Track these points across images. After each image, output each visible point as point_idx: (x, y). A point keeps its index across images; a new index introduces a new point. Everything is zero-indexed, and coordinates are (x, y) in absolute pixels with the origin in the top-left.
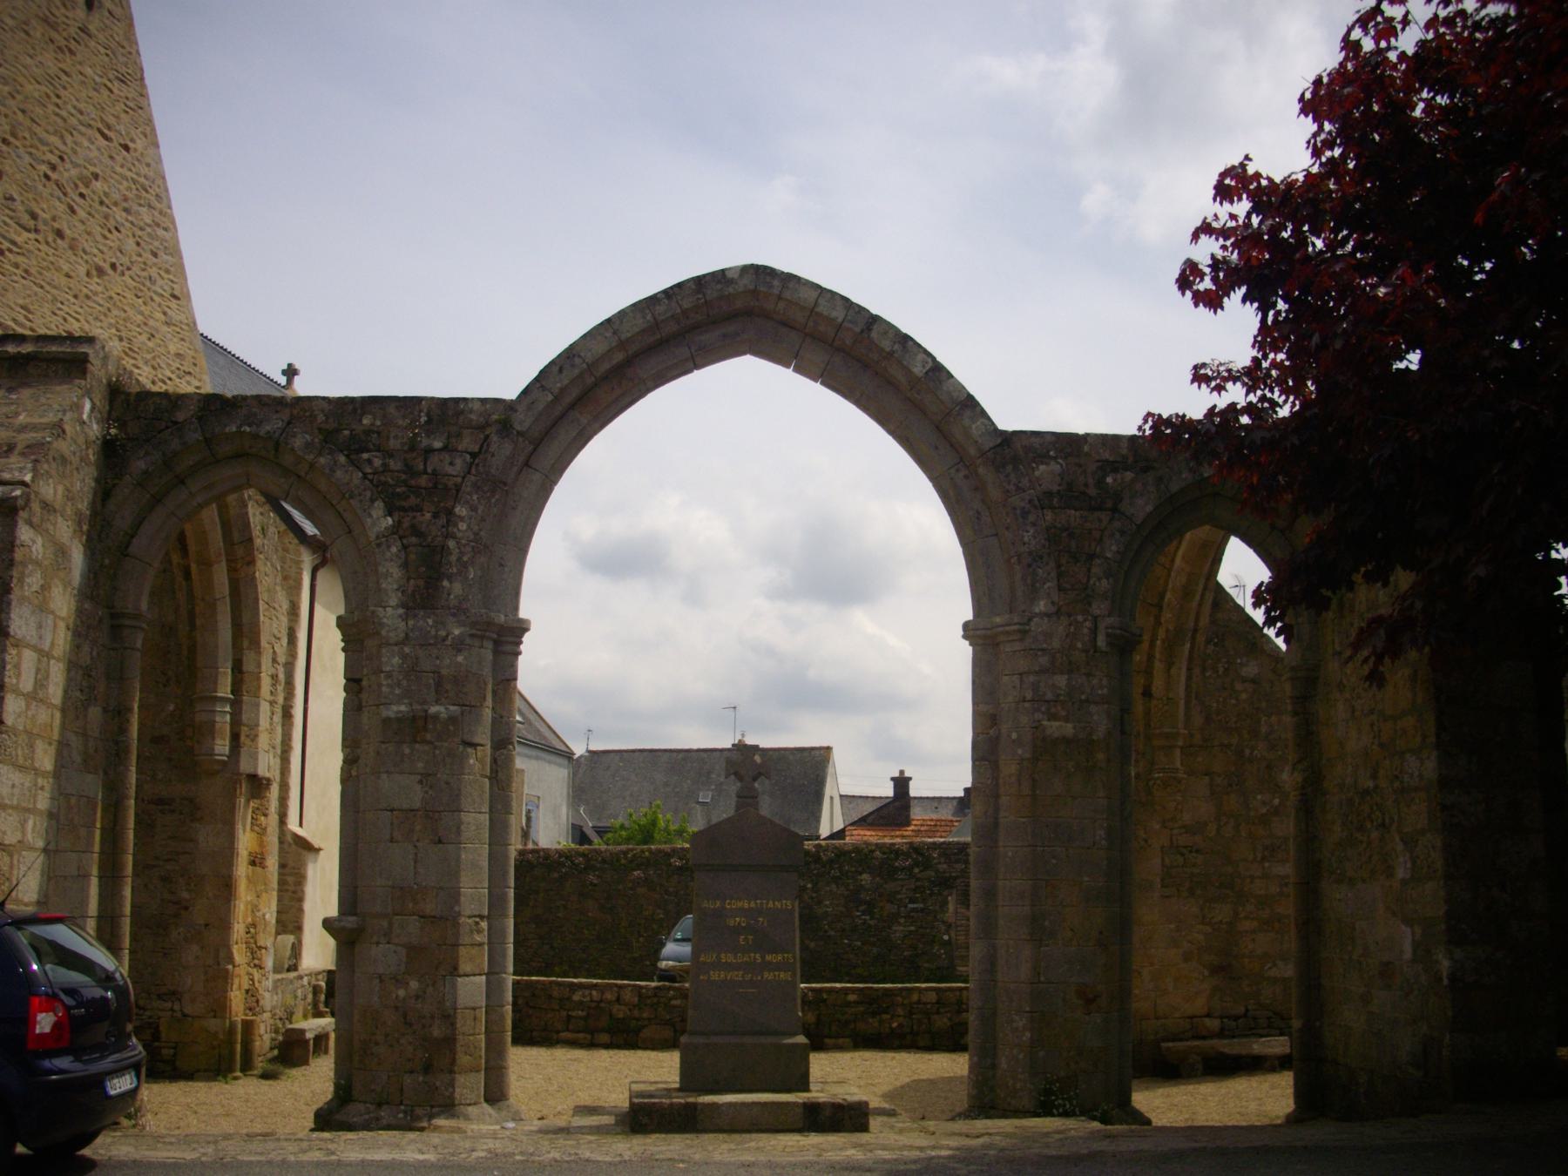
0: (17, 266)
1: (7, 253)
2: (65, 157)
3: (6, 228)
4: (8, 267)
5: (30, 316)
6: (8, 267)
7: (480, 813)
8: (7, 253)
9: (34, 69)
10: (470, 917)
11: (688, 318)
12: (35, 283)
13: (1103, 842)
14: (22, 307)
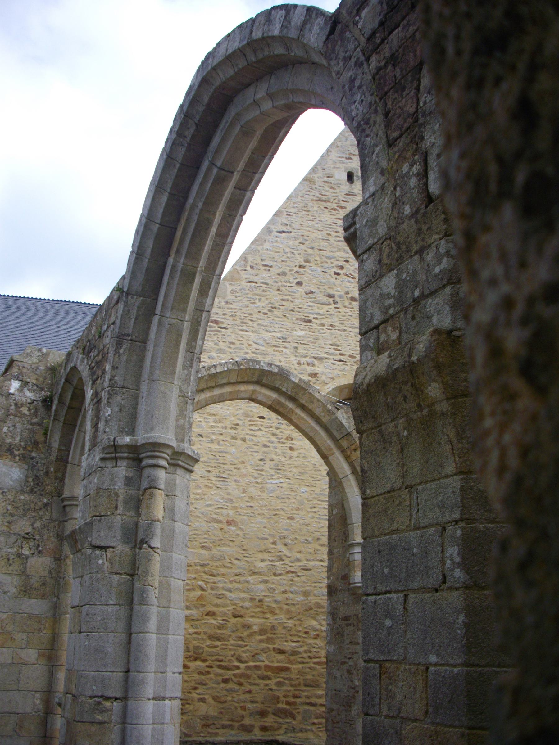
0: (323, 325)
1: (313, 321)
2: (348, 259)
3: (310, 308)
4: (317, 327)
5: (339, 348)
6: (317, 327)
7: (107, 605)
8: (313, 321)
9: (317, 225)
10: (91, 697)
11: (185, 137)
12: (339, 330)
13: (458, 573)
14: (331, 345)
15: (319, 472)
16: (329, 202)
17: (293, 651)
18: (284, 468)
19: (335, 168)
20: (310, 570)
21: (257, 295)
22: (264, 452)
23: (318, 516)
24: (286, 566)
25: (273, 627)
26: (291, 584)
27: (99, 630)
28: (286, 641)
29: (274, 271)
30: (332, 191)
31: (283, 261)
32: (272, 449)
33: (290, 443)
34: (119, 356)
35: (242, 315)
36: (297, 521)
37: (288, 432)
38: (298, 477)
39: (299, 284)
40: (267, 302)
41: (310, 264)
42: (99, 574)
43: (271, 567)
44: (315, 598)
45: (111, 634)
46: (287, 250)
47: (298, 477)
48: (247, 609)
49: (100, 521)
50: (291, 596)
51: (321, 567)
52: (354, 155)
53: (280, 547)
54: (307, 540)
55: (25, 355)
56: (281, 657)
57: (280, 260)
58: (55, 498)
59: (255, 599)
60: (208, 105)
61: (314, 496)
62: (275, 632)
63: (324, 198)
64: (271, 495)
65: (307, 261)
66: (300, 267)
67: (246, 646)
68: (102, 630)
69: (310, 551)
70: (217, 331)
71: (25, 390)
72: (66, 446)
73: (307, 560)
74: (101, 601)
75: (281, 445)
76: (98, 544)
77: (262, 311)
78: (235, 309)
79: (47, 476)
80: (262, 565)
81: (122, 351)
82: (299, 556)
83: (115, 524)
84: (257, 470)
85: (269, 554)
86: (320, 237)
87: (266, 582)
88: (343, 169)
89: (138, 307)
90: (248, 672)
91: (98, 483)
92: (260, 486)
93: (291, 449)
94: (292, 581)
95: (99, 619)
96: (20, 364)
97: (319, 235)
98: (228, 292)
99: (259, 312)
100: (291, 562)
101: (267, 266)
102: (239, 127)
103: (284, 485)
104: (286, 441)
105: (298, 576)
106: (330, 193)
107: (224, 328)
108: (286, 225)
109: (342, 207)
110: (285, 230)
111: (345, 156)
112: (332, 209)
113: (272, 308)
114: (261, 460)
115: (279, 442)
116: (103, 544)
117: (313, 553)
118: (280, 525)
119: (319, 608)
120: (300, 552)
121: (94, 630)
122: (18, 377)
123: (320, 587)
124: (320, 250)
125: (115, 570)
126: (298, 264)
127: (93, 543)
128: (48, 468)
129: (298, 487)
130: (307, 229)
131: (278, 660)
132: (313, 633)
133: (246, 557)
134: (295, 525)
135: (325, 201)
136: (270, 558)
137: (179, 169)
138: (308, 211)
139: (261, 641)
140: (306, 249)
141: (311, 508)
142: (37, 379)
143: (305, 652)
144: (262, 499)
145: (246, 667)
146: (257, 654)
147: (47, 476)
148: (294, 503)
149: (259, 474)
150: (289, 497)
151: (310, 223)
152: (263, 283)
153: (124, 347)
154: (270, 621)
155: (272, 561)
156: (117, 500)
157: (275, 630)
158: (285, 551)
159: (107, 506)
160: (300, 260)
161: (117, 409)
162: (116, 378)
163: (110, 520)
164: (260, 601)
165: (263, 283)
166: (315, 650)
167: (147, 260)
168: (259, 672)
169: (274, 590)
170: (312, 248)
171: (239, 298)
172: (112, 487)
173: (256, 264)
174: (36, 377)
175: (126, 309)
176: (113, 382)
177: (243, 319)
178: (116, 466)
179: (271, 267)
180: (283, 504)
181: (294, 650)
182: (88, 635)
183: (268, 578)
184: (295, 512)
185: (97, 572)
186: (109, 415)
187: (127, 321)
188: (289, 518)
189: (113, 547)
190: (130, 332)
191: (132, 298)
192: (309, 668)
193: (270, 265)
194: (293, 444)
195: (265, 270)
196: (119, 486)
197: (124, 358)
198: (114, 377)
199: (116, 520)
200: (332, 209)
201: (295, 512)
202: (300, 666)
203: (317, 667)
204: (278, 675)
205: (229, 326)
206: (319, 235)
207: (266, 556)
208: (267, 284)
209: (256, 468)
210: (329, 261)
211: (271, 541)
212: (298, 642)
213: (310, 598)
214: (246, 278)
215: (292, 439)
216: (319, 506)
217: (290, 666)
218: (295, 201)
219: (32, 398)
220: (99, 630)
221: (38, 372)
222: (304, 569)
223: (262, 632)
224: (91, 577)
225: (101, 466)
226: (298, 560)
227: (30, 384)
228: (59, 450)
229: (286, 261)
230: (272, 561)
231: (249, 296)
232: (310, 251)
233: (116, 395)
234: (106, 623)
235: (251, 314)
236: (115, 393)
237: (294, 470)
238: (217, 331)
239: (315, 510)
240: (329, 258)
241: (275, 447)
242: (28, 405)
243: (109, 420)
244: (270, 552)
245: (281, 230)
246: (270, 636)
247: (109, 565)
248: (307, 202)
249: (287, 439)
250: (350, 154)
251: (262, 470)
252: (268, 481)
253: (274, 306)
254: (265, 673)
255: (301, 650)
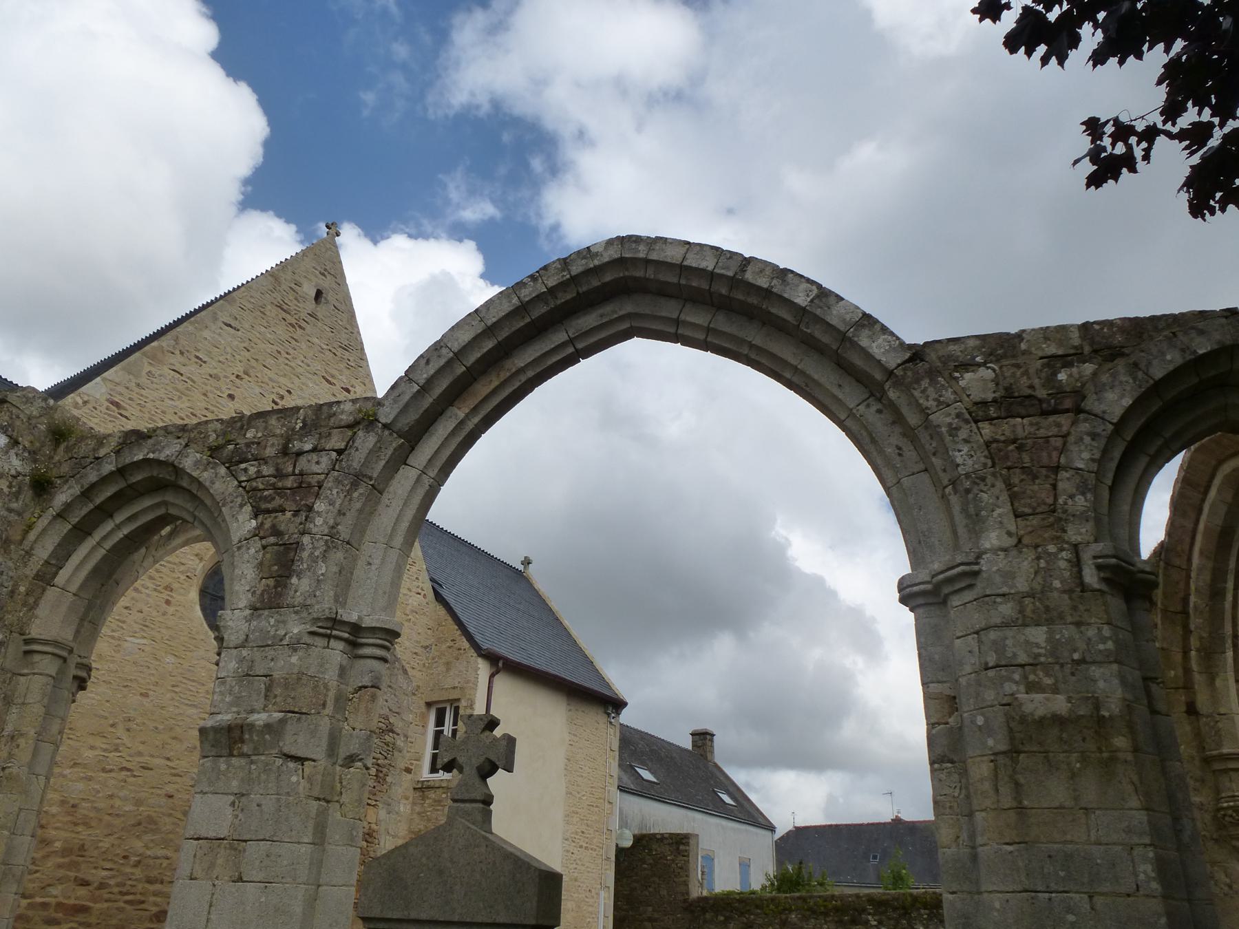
7: (299, 843)
15: (195, 641)
16: (289, 314)
17: (101, 883)
18: (153, 626)
19: (305, 277)
20: (151, 769)
21: (178, 391)
22: (133, 599)
23: (178, 698)
24: (121, 760)
25: (83, 845)
26: (123, 786)
27: (284, 881)
28: (95, 868)
29: (206, 369)
30: (296, 302)
31: (220, 362)
32: (143, 596)
33: (168, 595)
34: (350, 500)
35: (152, 408)
36: (152, 701)
37: (170, 580)
38: (167, 642)
39: (231, 397)
40: (188, 405)
41: (250, 379)
42: (290, 796)
43: (101, 758)
44: (149, 809)
45: (302, 886)
46: (229, 349)
47: (167, 642)
48: (53, 816)
49: (299, 719)
50: (118, 803)
51: (166, 768)
52: (329, 273)
53: (120, 732)
54: (157, 728)
55: (24, 400)
56: (82, 892)
57: (217, 359)
58: (15, 635)
59: (68, 803)
60: (605, 285)
61: (180, 671)
62: (84, 853)
63: (285, 307)
64: (127, 658)
65: (246, 373)
66: (238, 376)
67: (36, 872)
68: (289, 880)
69: (157, 743)
70: (116, 418)
71: (12, 452)
72: (58, 559)
73: (152, 756)
74: (290, 837)
75: (156, 594)
76: (293, 753)
77: (179, 414)
78: (147, 397)
79: (12, 597)
80: (90, 754)
81: (356, 495)
82: (141, 748)
83: (321, 728)
84: (118, 620)
85: (104, 740)
86: (269, 351)
87: (90, 779)
88: (313, 284)
89: (395, 449)
90: (30, 913)
91: (301, 665)
92: (116, 643)
93: (168, 602)
94: (125, 781)
95: (285, 863)
96: (14, 410)
97: (269, 349)
98: (144, 373)
99: (176, 413)
100: (130, 756)
101: (201, 359)
102: (628, 325)
103: (147, 649)
104: (163, 591)
105: (135, 776)
106: (292, 305)
107: (126, 417)
108: (236, 319)
109: (300, 327)
110: (233, 325)
111: (319, 269)
112: (290, 324)
113: (192, 413)
114: (126, 608)
115: (155, 590)
116: (300, 754)
117: (161, 746)
118: (128, 702)
119: (150, 824)
120: (143, 743)
121: (276, 880)
122: (7, 430)
123: (158, 795)
124: (265, 366)
125: (316, 793)
126: (236, 373)
127: (286, 750)
128: (16, 586)
129: (163, 654)
130: (258, 335)
131: (81, 895)
132: (134, 859)
133: (71, 739)
134: (147, 705)
135: (285, 311)
136: (104, 746)
137: (527, 325)
138: (265, 314)
139: (60, 866)
140: (250, 359)
141: (173, 686)
142: (31, 442)
143: (118, 885)
144: (113, 662)
145: (29, 904)
146: (49, 885)
147: (12, 597)
148: (153, 674)
149: (118, 626)
150: (150, 665)
151: (263, 329)
152: (189, 378)
153: (361, 491)
154: (82, 837)
155: (105, 750)
156: (326, 695)
157: (85, 851)
158: (126, 739)
159: (312, 701)
160: (239, 369)
161: (335, 569)
162: (339, 527)
163: (314, 722)
164: (73, 806)
165: (189, 378)
166: (130, 882)
167: (431, 400)
168: (45, 913)
169: (98, 792)
170: (257, 360)
171: (155, 386)
172: (321, 676)
173: (188, 351)
174: (30, 438)
175: (378, 445)
176: (335, 531)
177: (153, 415)
178: (328, 647)
179: (205, 362)
180: (139, 674)
181: (104, 881)
182: (266, 887)
183: (93, 775)
184: (152, 687)
185: (288, 794)
186: (322, 574)
187: (374, 460)
188: (141, 694)
189: (314, 761)
190: (375, 475)
191: (391, 434)
192: (117, 909)
193: (204, 360)
194: (172, 597)
195: (196, 363)
196: (331, 676)
197: (358, 505)
198: (337, 525)
199: (322, 723)
200: (290, 324)
201: (152, 687)
202: (106, 905)
203: (128, 907)
204: (72, 918)
205: (134, 418)
206: (269, 349)
207: (99, 742)
208: (194, 382)
209: (117, 618)
210: (270, 383)
211: (111, 722)
212: (111, 869)
213: (141, 809)
214: (171, 364)
215: (171, 590)
216: (184, 686)
217: (91, 904)
218: (252, 294)
219: (19, 469)
220: (284, 881)
221: (36, 432)
222: (143, 767)
223: (66, 852)
224: (278, 800)
225: (308, 642)
226: (140, 754)
227: (21, 447)
228: (47, 562)
229: (223, 363)
230: (105, 750)
231: (168, 388)
232: (253, 363)
233: (334, 550)
234: (295, 869)
235: (164, 412)
236: (335, 547)
237: (164, 631)
238: (116, 418)
239: (177, 689)
240: (270, 379)
241: (148, 595)
242: (10, 478)
243: (322, 580)
244: (104, 737)
245: (228, 322)
246: (74, 858)
247: (308, 786)
248: (265, 302)
249: (166, 588)
250: (325, 270)
251: (124, 622)
252: (128, 639)
253: (195, 413)
254: (54, 915)
255: (112, 882)
